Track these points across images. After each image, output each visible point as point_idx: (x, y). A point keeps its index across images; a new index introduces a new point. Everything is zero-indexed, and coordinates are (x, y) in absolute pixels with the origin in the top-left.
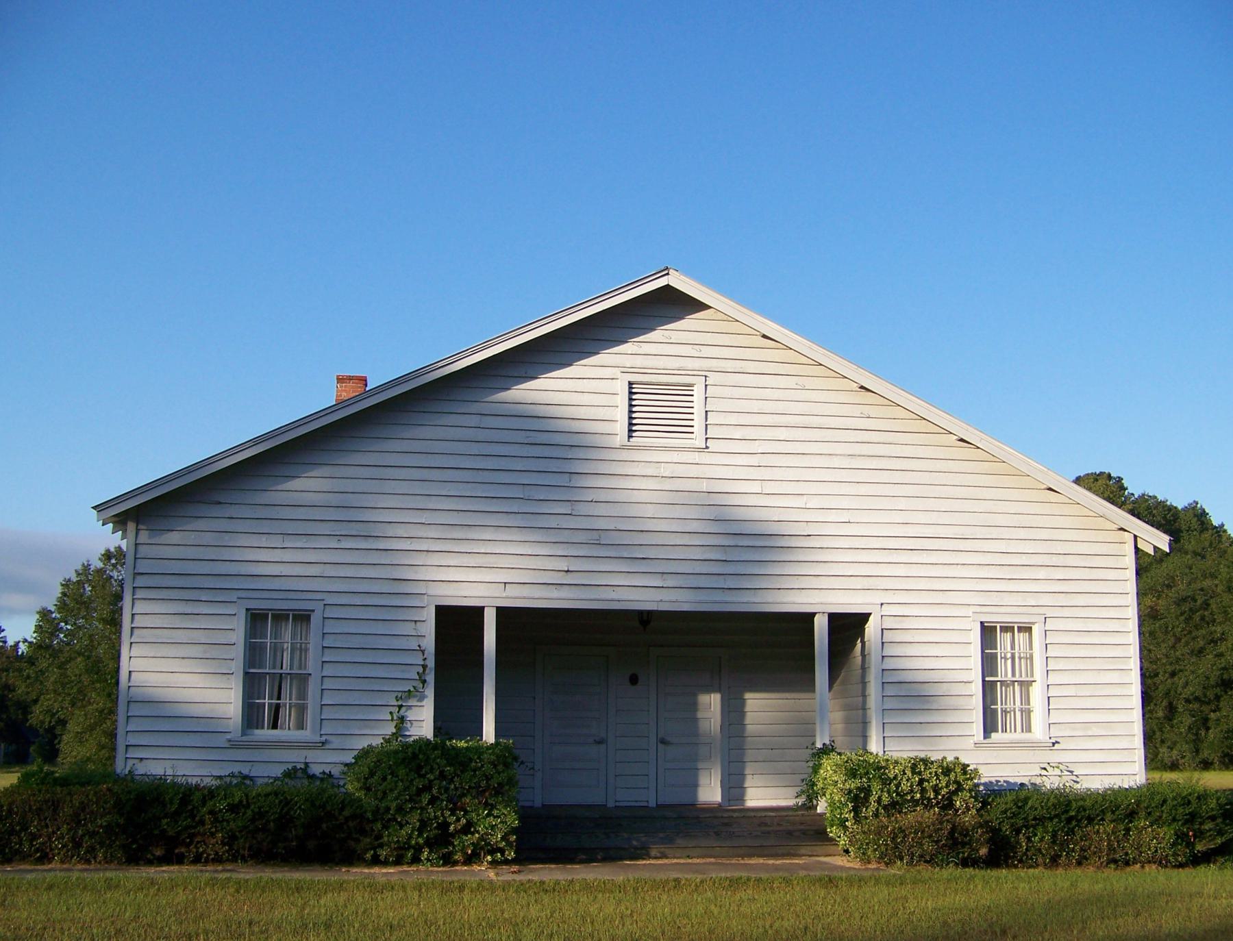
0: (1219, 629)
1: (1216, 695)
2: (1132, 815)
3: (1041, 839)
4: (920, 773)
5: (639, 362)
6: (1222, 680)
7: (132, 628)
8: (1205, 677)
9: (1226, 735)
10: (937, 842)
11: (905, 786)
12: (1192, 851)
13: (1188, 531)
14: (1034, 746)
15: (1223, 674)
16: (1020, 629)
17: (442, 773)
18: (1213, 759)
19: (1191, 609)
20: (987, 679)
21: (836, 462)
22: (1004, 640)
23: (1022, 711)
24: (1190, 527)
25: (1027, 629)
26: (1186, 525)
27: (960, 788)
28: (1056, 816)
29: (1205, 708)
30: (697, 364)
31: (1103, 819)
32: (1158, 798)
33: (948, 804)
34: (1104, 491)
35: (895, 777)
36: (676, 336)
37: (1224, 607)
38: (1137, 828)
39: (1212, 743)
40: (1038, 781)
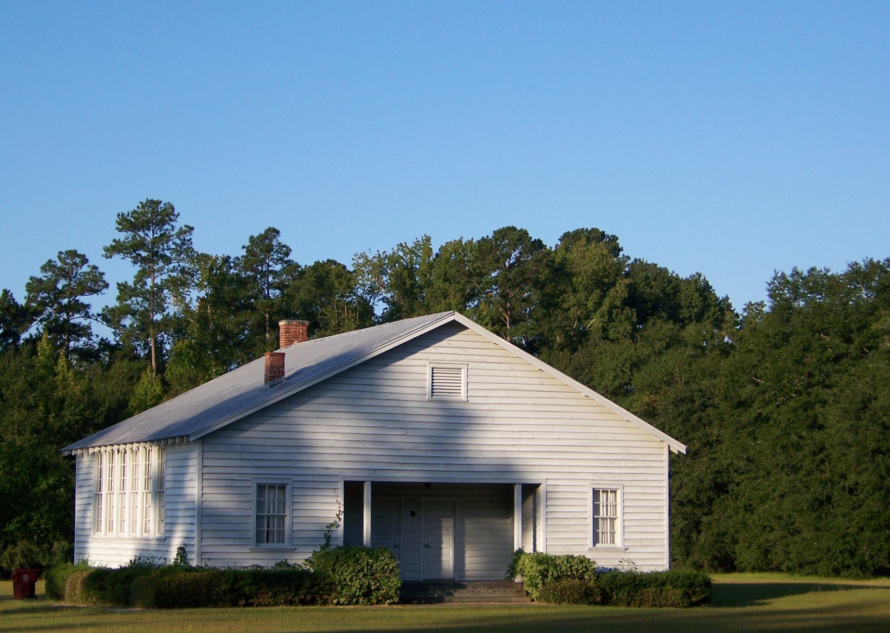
0: (715, 431)
1: (709, 498)
2: (663, 584)
3: (623, 594)
4: (570, 563)
5: (436, 357)
6: (716, 484)
7: (203, 494)
8: (699, 480)
9: (716, 539)
10: (580, 594)
11: (564, 568)
12: (690, 601)
13: (689, 307)
14: (617, 550)
15: (716, 478)
16: (611, 492)
18: (703, 563)
19: (688, 410)
20: (595, 517)
21: (527, 408)
22: (602, 496)
23: (610, 533)
24: (690, 303)
25: (615, 492)
26: (686, 300)
27: (587, 570)
28: (630, 583)
29: (698, 511)
30: (464, 358)
31: (650, 586)
32: (676, 576)
33: (581, 578)
34: (599, 262)
35: (560, 564)
36: (454, 344)
37: (720, 414)
38: (666, 590)
39: (703, 546)
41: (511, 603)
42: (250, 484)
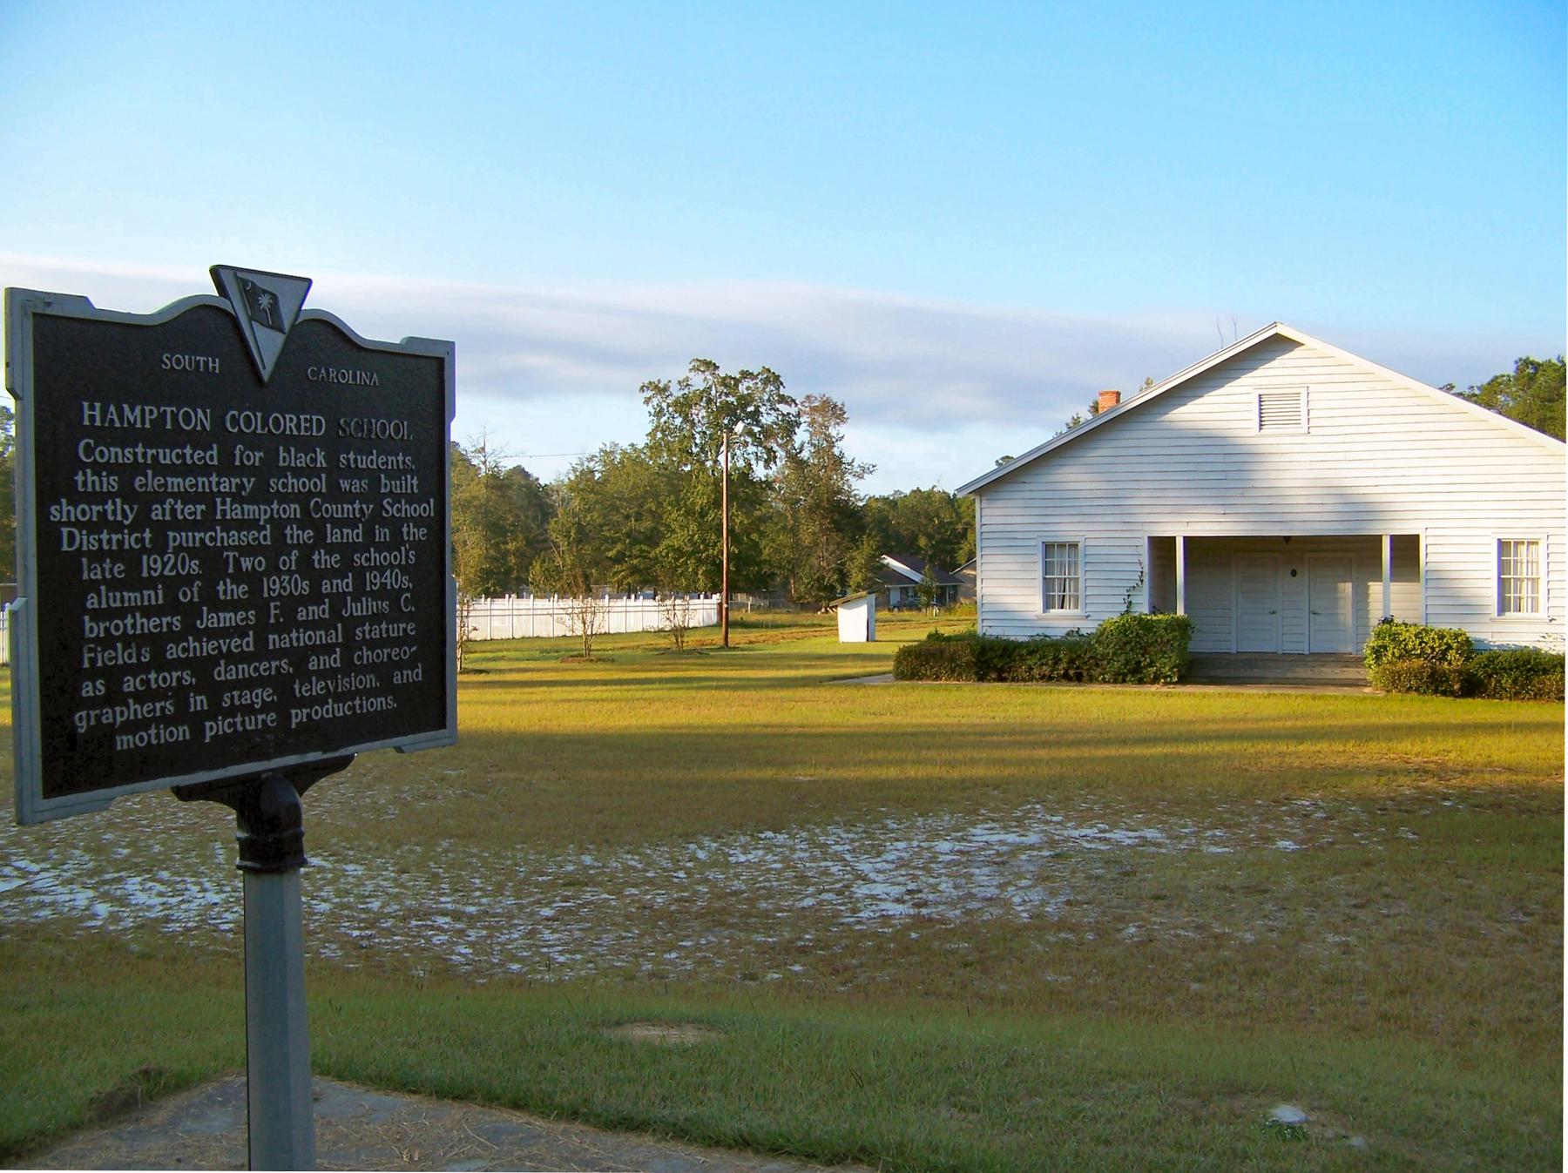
3: (1506, 681)
17: (1137, 634)
40: (1538, 645)
41: (752, 653)
42: (1033, 543)
